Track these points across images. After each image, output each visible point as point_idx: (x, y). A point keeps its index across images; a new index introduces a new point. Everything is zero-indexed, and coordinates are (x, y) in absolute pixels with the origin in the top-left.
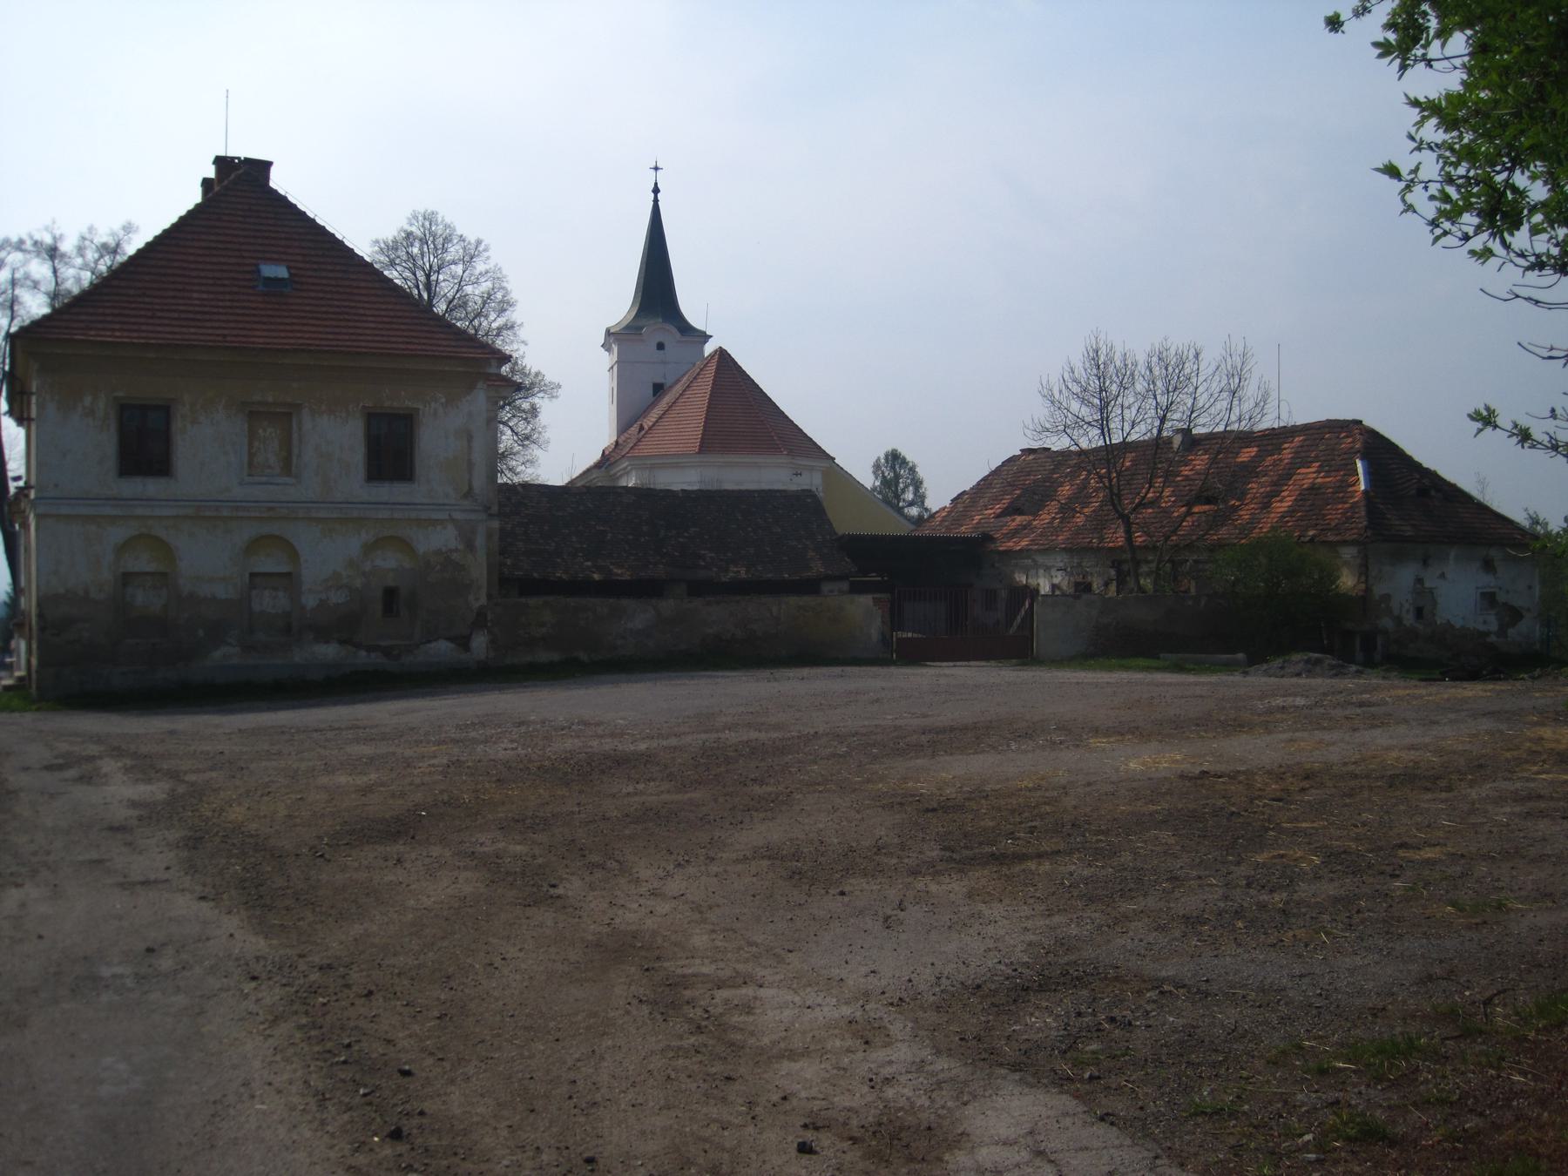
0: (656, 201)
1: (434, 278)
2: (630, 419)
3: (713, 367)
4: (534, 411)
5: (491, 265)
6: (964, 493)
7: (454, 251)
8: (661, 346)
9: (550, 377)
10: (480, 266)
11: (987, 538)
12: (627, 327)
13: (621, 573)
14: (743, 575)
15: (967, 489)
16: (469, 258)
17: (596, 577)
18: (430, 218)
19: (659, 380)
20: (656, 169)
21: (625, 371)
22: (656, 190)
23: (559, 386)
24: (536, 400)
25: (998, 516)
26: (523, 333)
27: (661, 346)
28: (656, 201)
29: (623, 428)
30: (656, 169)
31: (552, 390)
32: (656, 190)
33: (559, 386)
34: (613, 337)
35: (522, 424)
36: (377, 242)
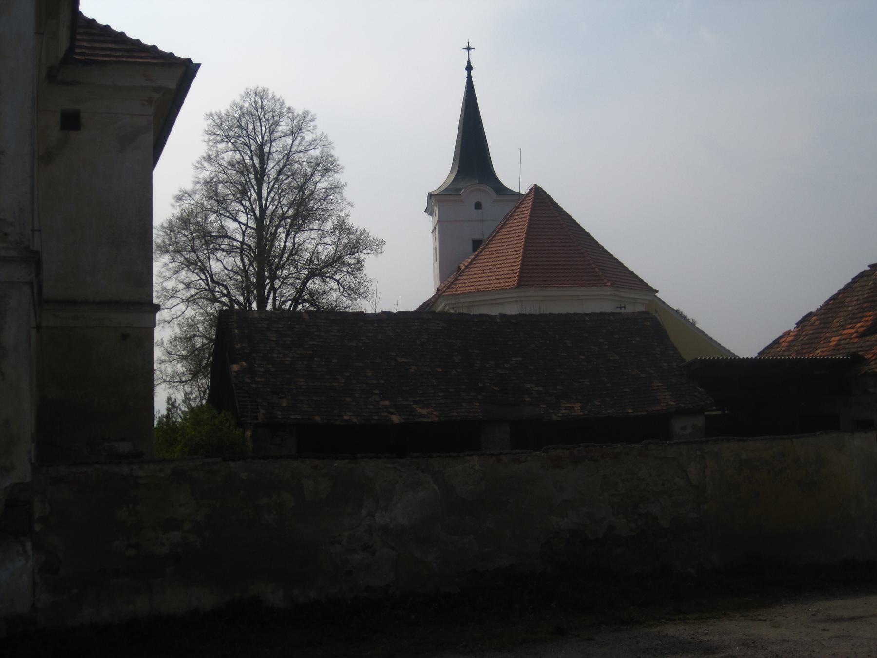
0: (469, 77)
1: (266, 149)
2: (451, 269)
3: (529, 203)
4: (359, 266)
5: (318, 132)
6: (810, 314)
7: (284, 126)
8: (478, 206)
9: (375, 233)
10: (308, 137)
11: (857, 359)
12: (446, 189)
13: (427, 414)
14: (578, 411)
15: (814, 310)
16: (295, 131)
17: (395, 419)
18: (261, 94)
19: (478, 237)
20: (469, 49)
21: (446, 232)
22: (469, 68)
23: (383, 242)
24: (362, 256)
25: (862, 335)
26: (347, 193)
27: (478, 206)
28: (469, 77)
29: (443, 277)
30: (469, 49)
31: (375, 246)
32: (469, 68)
33: (383, 242)
34: (435, 199)
35: (349, 278)
36: (210, 115)
